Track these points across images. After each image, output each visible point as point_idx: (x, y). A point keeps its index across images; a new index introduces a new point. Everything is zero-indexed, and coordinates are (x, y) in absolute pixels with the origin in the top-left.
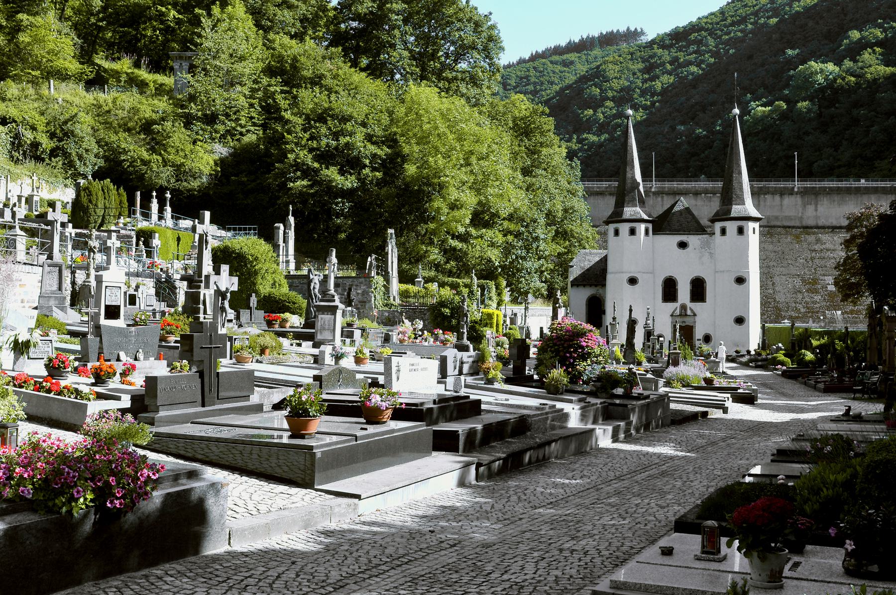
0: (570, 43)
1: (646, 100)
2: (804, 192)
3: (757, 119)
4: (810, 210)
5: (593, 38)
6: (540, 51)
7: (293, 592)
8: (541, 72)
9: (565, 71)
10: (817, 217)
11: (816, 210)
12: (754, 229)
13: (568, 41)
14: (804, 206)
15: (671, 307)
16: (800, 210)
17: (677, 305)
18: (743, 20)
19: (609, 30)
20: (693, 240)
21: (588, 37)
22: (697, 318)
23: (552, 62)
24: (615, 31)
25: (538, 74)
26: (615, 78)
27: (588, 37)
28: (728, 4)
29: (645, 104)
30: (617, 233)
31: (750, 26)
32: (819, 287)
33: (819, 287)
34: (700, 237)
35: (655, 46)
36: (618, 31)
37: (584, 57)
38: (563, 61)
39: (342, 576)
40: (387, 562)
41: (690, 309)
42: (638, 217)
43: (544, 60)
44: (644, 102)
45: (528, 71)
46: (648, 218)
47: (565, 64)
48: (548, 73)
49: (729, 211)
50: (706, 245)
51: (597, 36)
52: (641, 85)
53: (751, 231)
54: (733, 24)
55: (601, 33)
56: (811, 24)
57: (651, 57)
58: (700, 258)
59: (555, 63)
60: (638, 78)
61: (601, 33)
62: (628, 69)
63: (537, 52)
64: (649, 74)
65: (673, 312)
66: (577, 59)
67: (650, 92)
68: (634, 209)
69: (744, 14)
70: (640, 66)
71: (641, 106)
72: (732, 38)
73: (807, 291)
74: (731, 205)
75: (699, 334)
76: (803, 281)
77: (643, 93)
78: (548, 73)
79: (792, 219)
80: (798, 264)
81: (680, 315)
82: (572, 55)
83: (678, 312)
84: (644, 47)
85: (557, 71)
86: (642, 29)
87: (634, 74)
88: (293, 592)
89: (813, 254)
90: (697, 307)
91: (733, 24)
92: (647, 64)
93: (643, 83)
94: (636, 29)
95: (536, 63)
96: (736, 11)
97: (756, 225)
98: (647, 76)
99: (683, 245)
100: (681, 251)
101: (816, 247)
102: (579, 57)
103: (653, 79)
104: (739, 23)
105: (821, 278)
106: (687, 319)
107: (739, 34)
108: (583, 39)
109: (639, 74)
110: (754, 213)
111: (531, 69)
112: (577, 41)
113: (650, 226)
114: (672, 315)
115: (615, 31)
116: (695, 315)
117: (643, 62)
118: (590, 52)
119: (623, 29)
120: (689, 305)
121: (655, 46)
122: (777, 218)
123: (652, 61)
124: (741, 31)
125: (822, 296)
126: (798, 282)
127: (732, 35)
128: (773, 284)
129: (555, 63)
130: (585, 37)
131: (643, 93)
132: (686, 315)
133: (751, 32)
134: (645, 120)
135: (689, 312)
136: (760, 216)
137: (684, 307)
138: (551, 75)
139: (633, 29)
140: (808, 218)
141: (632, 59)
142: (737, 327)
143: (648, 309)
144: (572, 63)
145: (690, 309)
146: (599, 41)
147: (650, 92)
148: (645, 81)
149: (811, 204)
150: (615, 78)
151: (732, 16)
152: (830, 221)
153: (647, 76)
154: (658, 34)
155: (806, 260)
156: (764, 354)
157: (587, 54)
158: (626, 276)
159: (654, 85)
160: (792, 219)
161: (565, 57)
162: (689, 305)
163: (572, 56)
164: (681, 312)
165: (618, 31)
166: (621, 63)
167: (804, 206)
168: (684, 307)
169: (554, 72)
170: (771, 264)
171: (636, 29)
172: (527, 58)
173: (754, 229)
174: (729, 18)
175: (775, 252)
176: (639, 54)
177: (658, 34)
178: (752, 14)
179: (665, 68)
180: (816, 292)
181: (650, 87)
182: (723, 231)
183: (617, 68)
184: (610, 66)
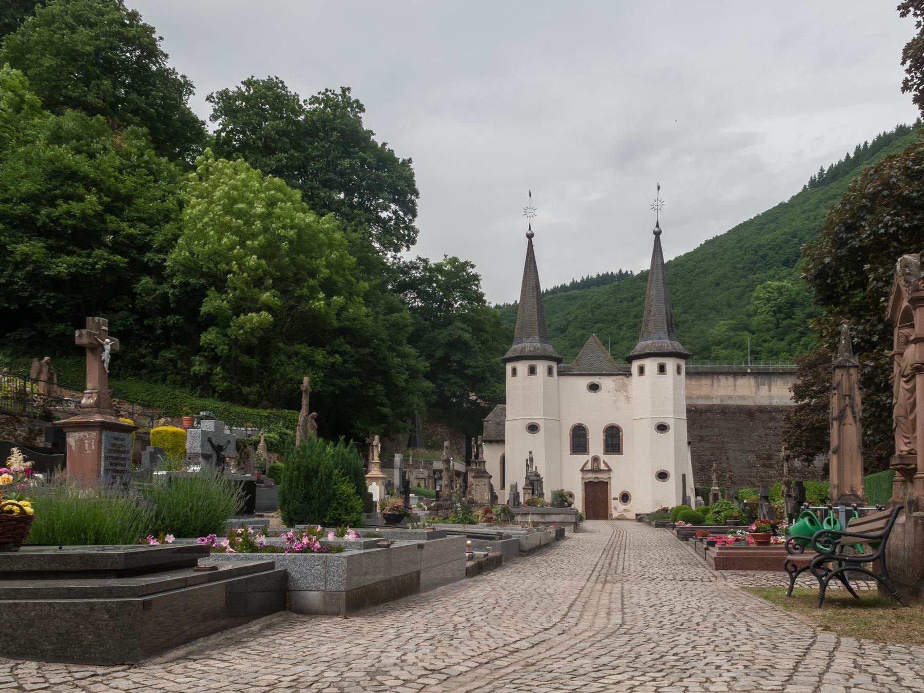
2: (756, 374)
4: (764, 390)
6: (549, 289)
7: (364, 688)
10: (771, 397)
11: (770, 390)
14: (758, 387)
15: (581, 460)
16: (754, 389)
17: (588, 457)
19: (605, 272)
20: (607, 383)
22: (612, 475)
27: (588, 278)
32: (774, 462)
33: (774, 462)
39: (426, 669)
40: (473, 656)
41: (604, 462)
50: (623, 388)
56: (771, 253)
65: (584, 466)
73: (762, 466)
75: (615, 491)
76: (758, 456)
79: (745, 399)
80: (752, 441)
88: (364, 688)
89: (767, 431)
90: (611, 460)
99: (594, 388)
101: (770, 425)
105: (776, 453)
114: (582, 470)
116: (609, 470)
119: (616, 272)
122: (730, 397)
125: (777, 471)
126: (752, 458)
128: (728, 458)
136: (687, 352)
137: (596, 459)
139: (624, 272)
140: (763, 397)
142: (660, 483)
145: (604, 462)
149: (764, 385)
152: (784, 401)
155: (760, 437)
160: (745, 399)
161: (568, 293)
162: (604, 458)
164: (592, 465)
167: (758, 387)
168: (596, 459)
170: (725, 440)
175: (729, 429)
180: (771, 467)
182: (642, 370)
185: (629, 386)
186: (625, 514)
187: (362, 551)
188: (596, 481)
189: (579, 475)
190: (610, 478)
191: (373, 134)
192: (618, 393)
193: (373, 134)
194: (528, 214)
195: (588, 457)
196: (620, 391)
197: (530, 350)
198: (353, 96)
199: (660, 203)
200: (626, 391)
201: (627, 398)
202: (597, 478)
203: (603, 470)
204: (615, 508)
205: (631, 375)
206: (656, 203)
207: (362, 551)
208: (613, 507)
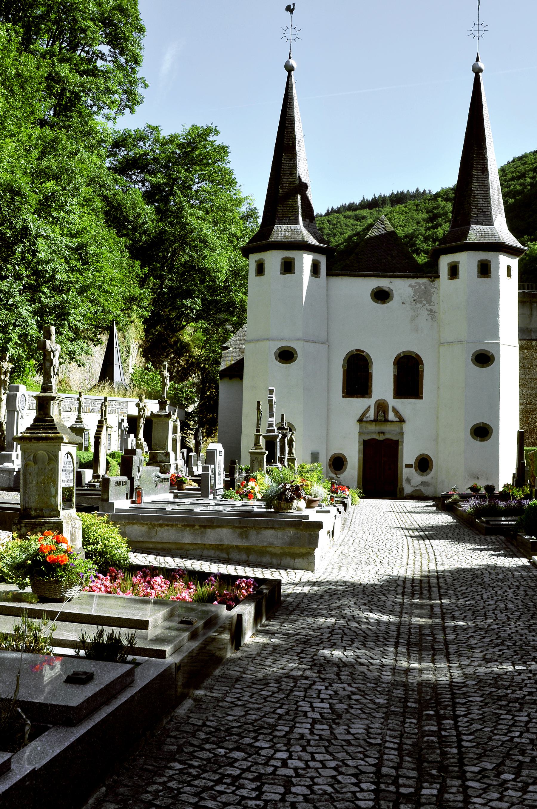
0: (363, 201)
1: (428, 246)
3: (533, 256)
5: (385, 197)
6: (335, 208)
8: (334, 225)
9: (356, 225)
12: (509, 268)
13: (361, 199)
17: (370, 402)
18: (523, 175)
19: (400, 191)
21: (380, 196)
22: (406, 427)
23: (345, 217)
24: (405, 192)
25: (331, 226)
26: (400, 226)
28: (509, 163)
29: (427, 249)
30: (260, 269)
31: (528, 180)
34: (413, 281)
35: (439, 199)
36: (408, 192)
37: (375, 213)
38: (356, 216)
41: (394, 410)
42: (299, 239)
43: (338, 215)
44: (425, 247)
45: (323, 223)
46: (316, 243)
47: (357, 218)
48: (341, 226)
49: (465, 234)
51: (388, 195)
52: (424, 232)
53: (503, 272)
54: (513, 179)
55: (392, 193)
57: (435, 208)
58: (413, 319)
59: (349, 217)
60: (422, 226)
61: (392, 193)
62: (412, 218)
63: (332, 208)
64: (432, 222)
66: (369, 215)
67: (433, 238)
68: (292, 227)
69: (523, 171)
70: (425, 216)
71: (423, 251)
72: (512, 190)
74: (469, 225)
77: (426, 239)
78: (341, 226)
81: (376, 420)
82: (365, 211)
83: (371, 415)
84: (429, 200)
85: (349, 224)
86: (430, 191)
87: (418, 223)
91: (513, 179)
92: (431, 214)
93: (426, 230)
94: (425, 191)
95: (331, 217)
96: (516, 168)
97: (514, 263)
98: (430, 225)
100: (378, 306)
102: (371, 213)
103: (435, 227)
104: (519, 178)
106: (387, 428)
107: (519, 187)
108: (375, 198)
109: (422, 222)
110: (510, 239)
111: (326, 222)
112: (370, 199)
113: (323, 260)
114: (360, 421)
115: (405, 192)
116: (402, 420)
117: (427, 213)
118: (381, 209)
119: (412, 190)
120: (392, 402)
121: (439, 199)
123: (437, 211)
124: (521, 185)
127: (512, 187)
129: (349, 217)
130: (377, 196)
131: (426, 239)
132: (386, 421)
133: (531, 184)
134: (426, 263)
135: (391, 416)
137: (382, 407)
138: (344, 227)
139: (421, 190)
141: (417, 210)
143: (271, 392)
144: (364, 218)
145: (394, 410)
146: (390, 200)
147: (433, 238)
148: (428, 229)
150: (400, 226)
151: (512, 172)
153: (430, 225)
154: (442, 188)
156: (518, 494)
157: (379, 211)
158: (275, 346)
159: (436, 232)
161: (357, 212)
162: (392, 402)
163: (365, 212)
165: (408, 192)
166: (406, 213)
168: (382, 407)
169: (346, 225)
171: (425, 191)
172: (324, 214)
173: (509, 268)
174: (509, 174)
176: (424, 205)
177: (442, 188)
178: (531, 170)
179: (447, 217)
181: (433, 233)
182: (454, 272)
183: (402, 217)
184: (396, 215)
185: (435, 295)
186: (423, 489)
187: (47, 520)
188: (381, 438)
189: (356, 428)
190: (402, 434)
191: (217, 133)
192: (418, 305)
193: (217, 133)
194: (289, 37)
195: (370, 402)
196: (421, 302)
197: (285, 236)
198: (218, 129)
199: (481, 28)
200: (429, 302)
201: (432, 312)
202: (383, 433)
203: (392, 421)
204: (408, 481)
205: (438, 277)
206: (476, 28)
207: (47, 520)
208: (405, 477)
